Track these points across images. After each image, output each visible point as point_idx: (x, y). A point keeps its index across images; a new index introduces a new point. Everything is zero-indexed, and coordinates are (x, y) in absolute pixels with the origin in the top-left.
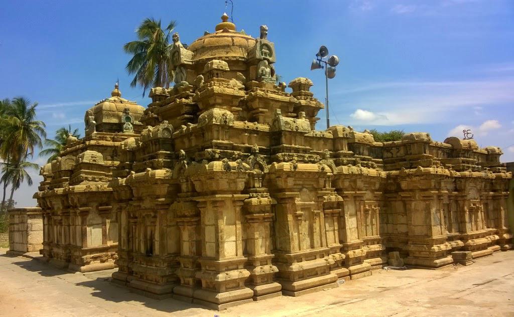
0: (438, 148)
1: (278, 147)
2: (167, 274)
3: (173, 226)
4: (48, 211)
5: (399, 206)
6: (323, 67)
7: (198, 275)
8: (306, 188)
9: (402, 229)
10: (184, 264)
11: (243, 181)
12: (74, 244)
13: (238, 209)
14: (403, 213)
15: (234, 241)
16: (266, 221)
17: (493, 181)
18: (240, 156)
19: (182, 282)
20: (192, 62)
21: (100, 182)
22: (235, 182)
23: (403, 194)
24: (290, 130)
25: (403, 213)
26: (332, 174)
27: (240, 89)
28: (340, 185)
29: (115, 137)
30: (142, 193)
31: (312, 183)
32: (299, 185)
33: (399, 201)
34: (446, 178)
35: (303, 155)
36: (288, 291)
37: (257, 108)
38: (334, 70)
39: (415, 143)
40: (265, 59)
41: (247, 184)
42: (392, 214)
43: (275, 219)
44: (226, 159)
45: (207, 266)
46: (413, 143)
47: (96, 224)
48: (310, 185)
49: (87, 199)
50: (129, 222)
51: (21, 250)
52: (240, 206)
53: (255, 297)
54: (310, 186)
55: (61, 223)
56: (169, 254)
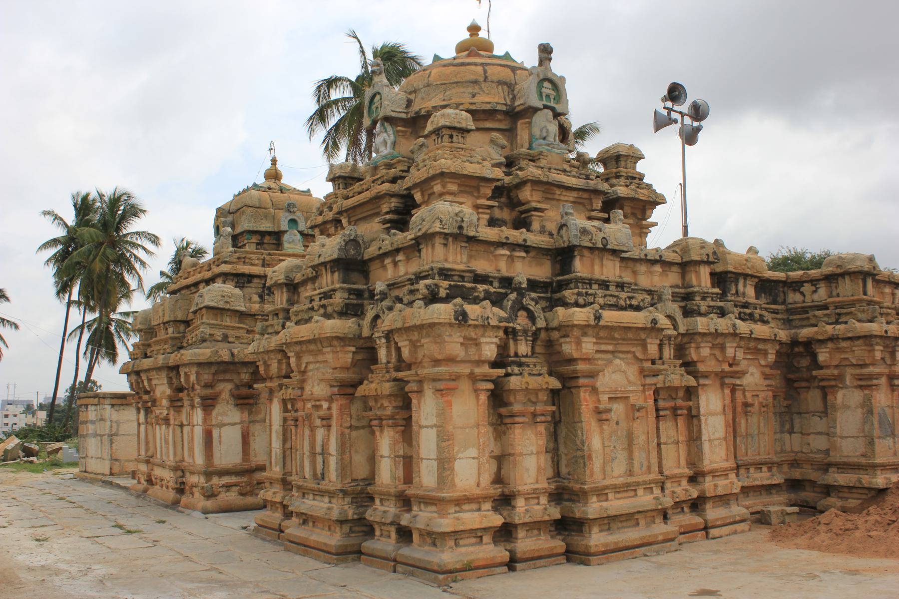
1: (566, 277)
2: (350, 518)
3: (363, 427)
4: (146, 397)
5: (813, 398)
6: (676, 121)
8: (620, 359)
9: (819, 443)
11: (492, 343)
12: (191, 461)
13: (483, 397)
14: (822, 412)
15: (473, 458)
18: (488, 296)
20: (407, 113)
21: (237, 345)
22: (478, 345)
24: (591, 245)
25: (822, 412)
26: (674, 333)
27: (498, 165)
28: (693, 355)
29: (267, 258)
33: (814, 388)
35: (617, 294)
36: (575, 555)
37: (528, 202)
38: (698, 129)
40: (546, 107)
41: (503, 348)
42: (800, 413)
43: (557, 418)
44: (458, 300)
49: (214, 374)
50: (285, 420)
51: (99, 471)
52: (488, 390)
53: (512, 564)
55: (166, 421)
56: (354, 480)
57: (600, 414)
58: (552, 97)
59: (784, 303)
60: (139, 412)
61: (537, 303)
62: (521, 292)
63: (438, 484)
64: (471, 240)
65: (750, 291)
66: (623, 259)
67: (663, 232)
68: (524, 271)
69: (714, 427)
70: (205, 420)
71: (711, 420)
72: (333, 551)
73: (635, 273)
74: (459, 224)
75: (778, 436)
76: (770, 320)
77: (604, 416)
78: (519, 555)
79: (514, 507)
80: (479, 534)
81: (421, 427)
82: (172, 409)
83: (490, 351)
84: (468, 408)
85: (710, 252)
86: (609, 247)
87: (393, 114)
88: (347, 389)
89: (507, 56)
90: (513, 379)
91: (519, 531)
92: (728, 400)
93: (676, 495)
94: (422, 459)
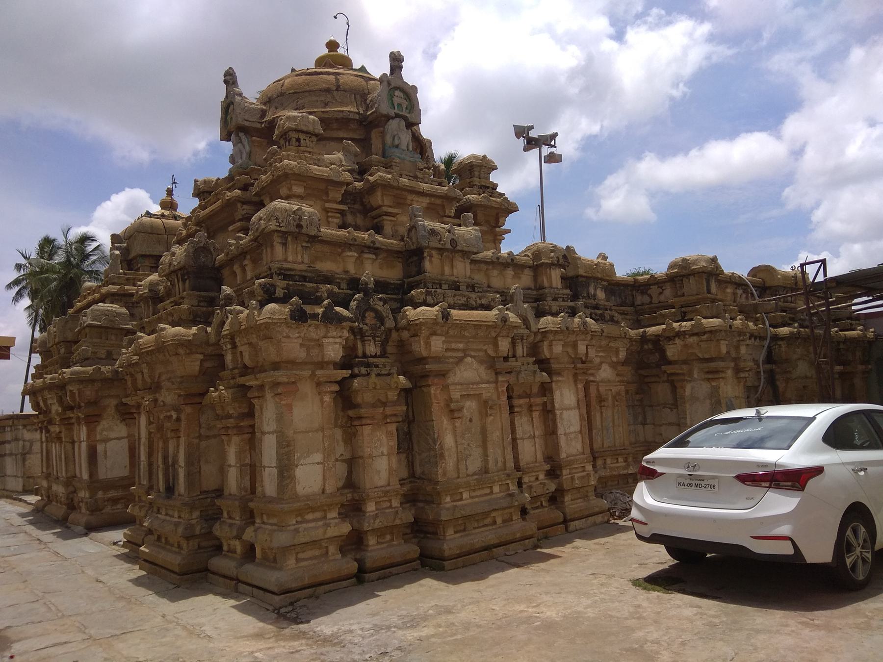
0: (736, 282)
1: (417, 278)
2: (197, 533)
5: (662, 391)
7: (249, 534)
8: (472, 357)
10: (228, 513)
11: (336, 343)
15: (318, 463)
16: (388, 420)
17: (842, 346)
19: (225, 548)
23: (669, 369)
24: (440, 246)
26: (526, 331)
28: (546, 353)
30: (160, 375)
31: (485, 347)
32: (458, 350)
33: (664, 382)
34: (750, 339)
37: (380, 207)
39: (689, 275)
40: (397, 116)
42: (652, 406)
45: (265, 516)
46: (688, 276)
47: (115, 439)
48: (480, 350)
52: (332, 392)
54: (481, 354)
55: (59, 439)
56: (202, 493)
57: (453, 413)
58: (404, 106)
59: (633, 305)
60: (41, 432)
61: (385, 304)
62: (367, 293)
63: (278, 494)
64: (314, 239)
65: (601, 294)
66: (473, 262)
67: (516, 241)
68: (370, 271)
69: (570, 421)
70: (88, 436)
71: (566, 414)
72: (177, 569)
73: (488, 276)
74: (297, 222)
75: (632, 427)
76: (620, 320)
77: (456, 415)
78: (368, 564)
79: (365, 512)
80: (324, 544)
81: (263, 433)
82: (63, 427)
83: (334, 350)
84: (310, 411)
85: (560, 255)
86: (458, 248)
87: (247, 124)
88: (196, 398)
89: (363, 69)
90: (356, 382)
91: (370, 538)
92: (582, 394)
93: (533, 490)
94: (264, 467)
